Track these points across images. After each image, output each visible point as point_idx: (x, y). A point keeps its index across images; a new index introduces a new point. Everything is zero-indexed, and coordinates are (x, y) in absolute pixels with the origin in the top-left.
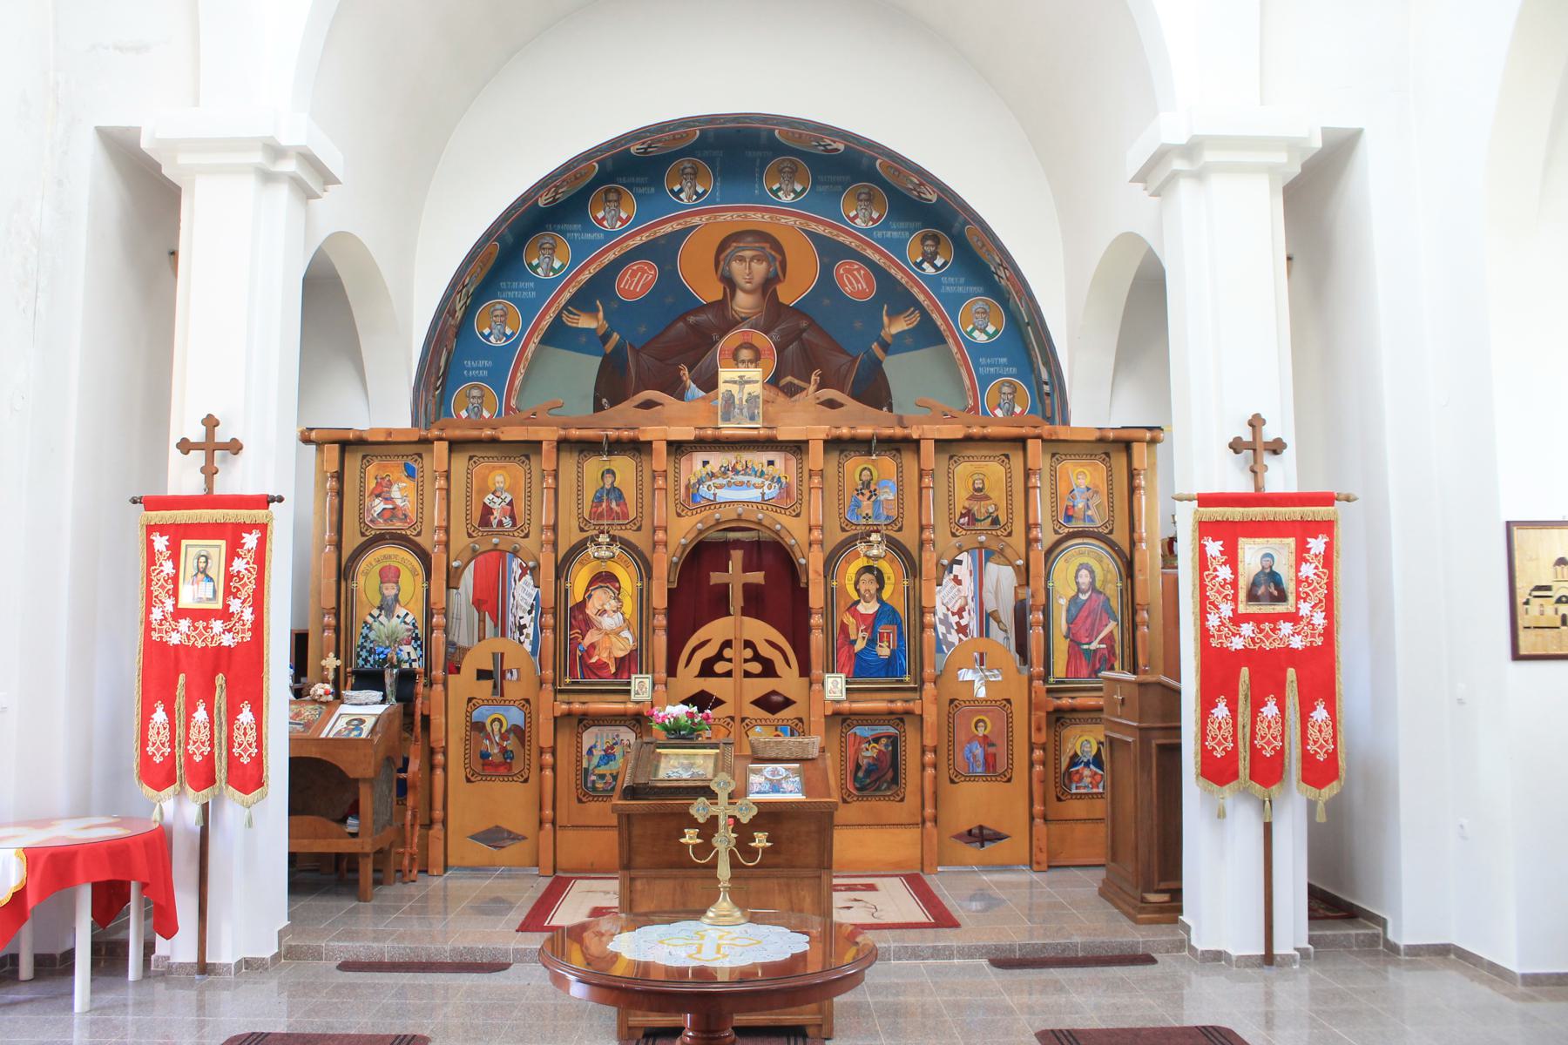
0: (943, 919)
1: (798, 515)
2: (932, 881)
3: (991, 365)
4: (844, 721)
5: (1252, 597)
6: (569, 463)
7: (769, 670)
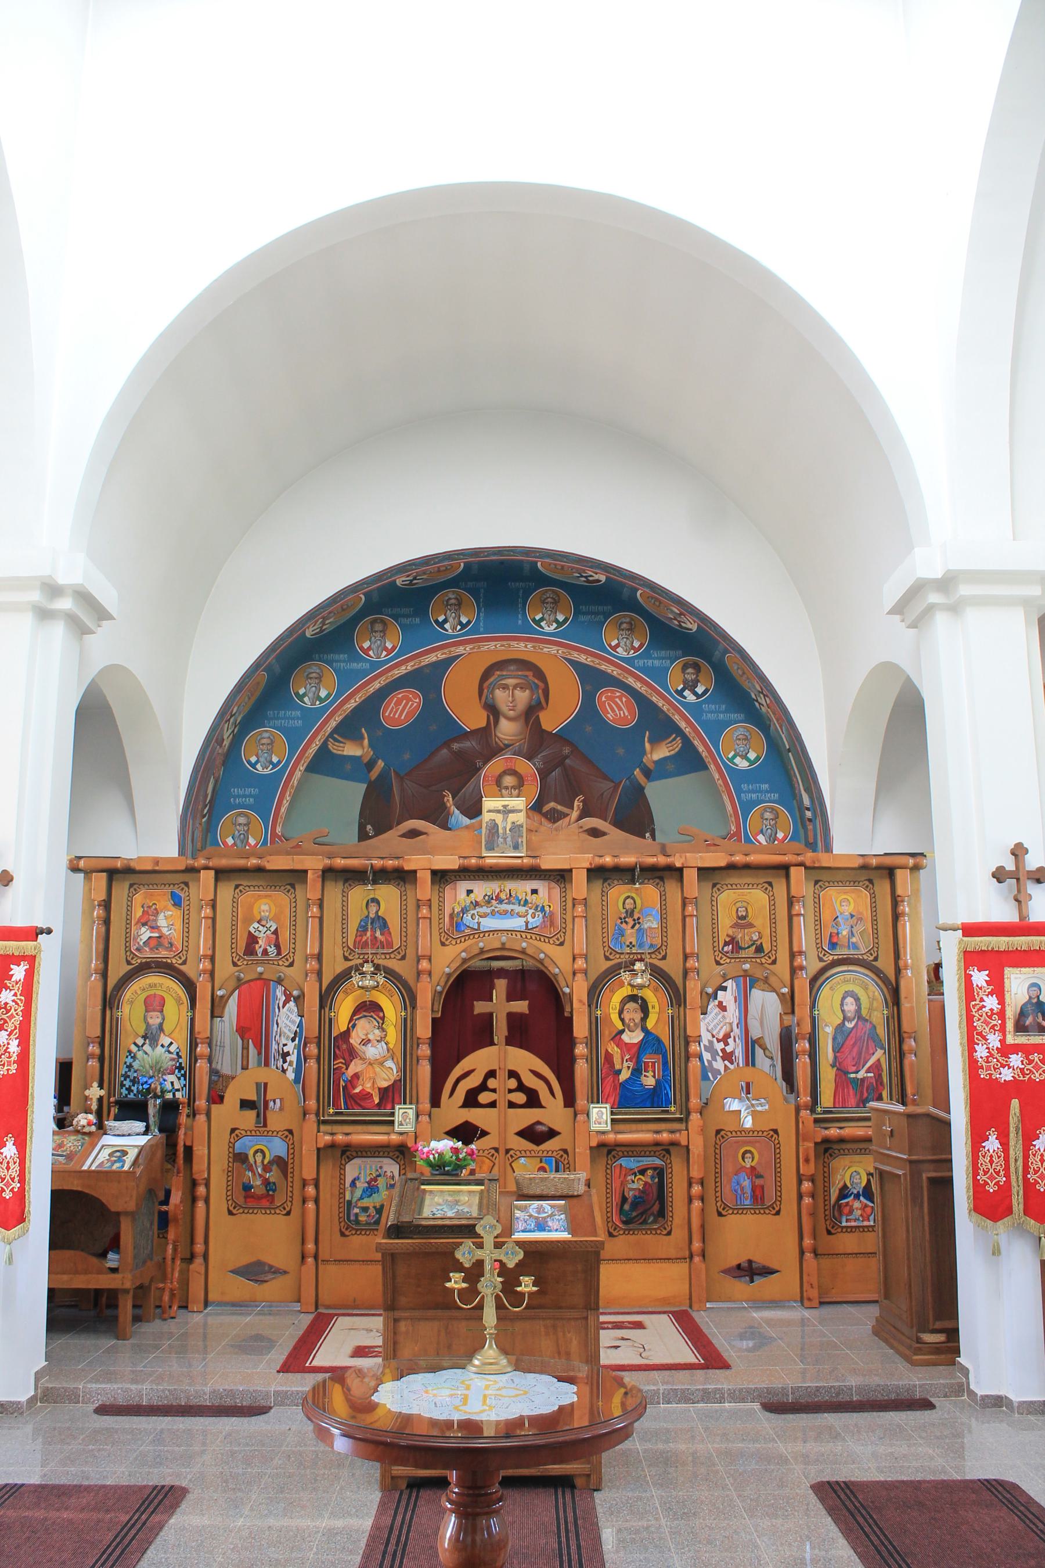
0: (712, 1360)
1: (562, 944)
2: (701, 1318)
3: (753, 791)
4: (609, 1152)
5: (1020, 1027)
6: (334, 892)
7: (533, 1101)
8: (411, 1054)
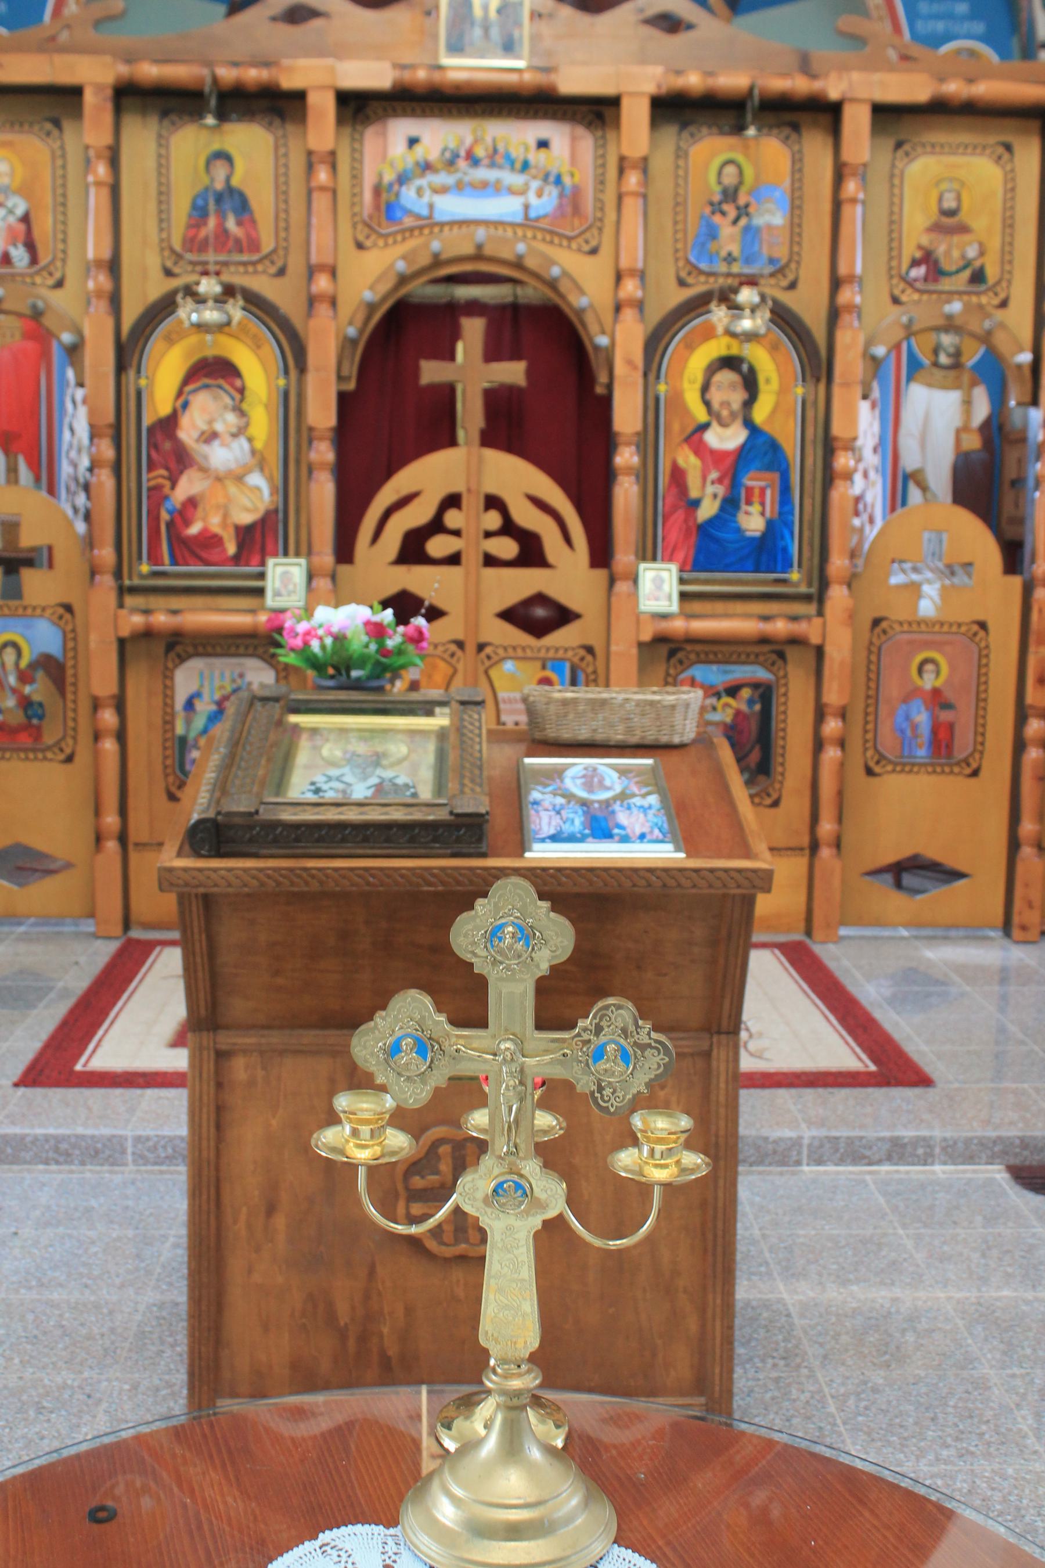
0: (893, 1067)
1: (594, 251)
2: (829, 953)
3: (937, 17)
4: (672, 653)
6: (141, 137)
7: (531, 553)
8: (298, 462)
